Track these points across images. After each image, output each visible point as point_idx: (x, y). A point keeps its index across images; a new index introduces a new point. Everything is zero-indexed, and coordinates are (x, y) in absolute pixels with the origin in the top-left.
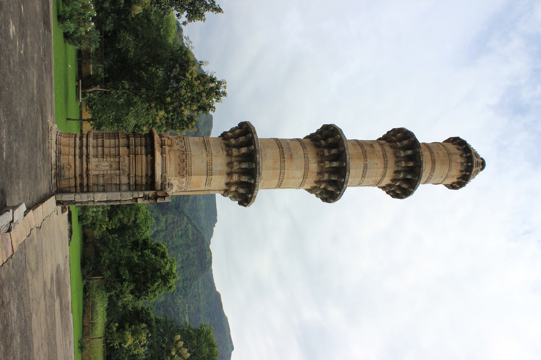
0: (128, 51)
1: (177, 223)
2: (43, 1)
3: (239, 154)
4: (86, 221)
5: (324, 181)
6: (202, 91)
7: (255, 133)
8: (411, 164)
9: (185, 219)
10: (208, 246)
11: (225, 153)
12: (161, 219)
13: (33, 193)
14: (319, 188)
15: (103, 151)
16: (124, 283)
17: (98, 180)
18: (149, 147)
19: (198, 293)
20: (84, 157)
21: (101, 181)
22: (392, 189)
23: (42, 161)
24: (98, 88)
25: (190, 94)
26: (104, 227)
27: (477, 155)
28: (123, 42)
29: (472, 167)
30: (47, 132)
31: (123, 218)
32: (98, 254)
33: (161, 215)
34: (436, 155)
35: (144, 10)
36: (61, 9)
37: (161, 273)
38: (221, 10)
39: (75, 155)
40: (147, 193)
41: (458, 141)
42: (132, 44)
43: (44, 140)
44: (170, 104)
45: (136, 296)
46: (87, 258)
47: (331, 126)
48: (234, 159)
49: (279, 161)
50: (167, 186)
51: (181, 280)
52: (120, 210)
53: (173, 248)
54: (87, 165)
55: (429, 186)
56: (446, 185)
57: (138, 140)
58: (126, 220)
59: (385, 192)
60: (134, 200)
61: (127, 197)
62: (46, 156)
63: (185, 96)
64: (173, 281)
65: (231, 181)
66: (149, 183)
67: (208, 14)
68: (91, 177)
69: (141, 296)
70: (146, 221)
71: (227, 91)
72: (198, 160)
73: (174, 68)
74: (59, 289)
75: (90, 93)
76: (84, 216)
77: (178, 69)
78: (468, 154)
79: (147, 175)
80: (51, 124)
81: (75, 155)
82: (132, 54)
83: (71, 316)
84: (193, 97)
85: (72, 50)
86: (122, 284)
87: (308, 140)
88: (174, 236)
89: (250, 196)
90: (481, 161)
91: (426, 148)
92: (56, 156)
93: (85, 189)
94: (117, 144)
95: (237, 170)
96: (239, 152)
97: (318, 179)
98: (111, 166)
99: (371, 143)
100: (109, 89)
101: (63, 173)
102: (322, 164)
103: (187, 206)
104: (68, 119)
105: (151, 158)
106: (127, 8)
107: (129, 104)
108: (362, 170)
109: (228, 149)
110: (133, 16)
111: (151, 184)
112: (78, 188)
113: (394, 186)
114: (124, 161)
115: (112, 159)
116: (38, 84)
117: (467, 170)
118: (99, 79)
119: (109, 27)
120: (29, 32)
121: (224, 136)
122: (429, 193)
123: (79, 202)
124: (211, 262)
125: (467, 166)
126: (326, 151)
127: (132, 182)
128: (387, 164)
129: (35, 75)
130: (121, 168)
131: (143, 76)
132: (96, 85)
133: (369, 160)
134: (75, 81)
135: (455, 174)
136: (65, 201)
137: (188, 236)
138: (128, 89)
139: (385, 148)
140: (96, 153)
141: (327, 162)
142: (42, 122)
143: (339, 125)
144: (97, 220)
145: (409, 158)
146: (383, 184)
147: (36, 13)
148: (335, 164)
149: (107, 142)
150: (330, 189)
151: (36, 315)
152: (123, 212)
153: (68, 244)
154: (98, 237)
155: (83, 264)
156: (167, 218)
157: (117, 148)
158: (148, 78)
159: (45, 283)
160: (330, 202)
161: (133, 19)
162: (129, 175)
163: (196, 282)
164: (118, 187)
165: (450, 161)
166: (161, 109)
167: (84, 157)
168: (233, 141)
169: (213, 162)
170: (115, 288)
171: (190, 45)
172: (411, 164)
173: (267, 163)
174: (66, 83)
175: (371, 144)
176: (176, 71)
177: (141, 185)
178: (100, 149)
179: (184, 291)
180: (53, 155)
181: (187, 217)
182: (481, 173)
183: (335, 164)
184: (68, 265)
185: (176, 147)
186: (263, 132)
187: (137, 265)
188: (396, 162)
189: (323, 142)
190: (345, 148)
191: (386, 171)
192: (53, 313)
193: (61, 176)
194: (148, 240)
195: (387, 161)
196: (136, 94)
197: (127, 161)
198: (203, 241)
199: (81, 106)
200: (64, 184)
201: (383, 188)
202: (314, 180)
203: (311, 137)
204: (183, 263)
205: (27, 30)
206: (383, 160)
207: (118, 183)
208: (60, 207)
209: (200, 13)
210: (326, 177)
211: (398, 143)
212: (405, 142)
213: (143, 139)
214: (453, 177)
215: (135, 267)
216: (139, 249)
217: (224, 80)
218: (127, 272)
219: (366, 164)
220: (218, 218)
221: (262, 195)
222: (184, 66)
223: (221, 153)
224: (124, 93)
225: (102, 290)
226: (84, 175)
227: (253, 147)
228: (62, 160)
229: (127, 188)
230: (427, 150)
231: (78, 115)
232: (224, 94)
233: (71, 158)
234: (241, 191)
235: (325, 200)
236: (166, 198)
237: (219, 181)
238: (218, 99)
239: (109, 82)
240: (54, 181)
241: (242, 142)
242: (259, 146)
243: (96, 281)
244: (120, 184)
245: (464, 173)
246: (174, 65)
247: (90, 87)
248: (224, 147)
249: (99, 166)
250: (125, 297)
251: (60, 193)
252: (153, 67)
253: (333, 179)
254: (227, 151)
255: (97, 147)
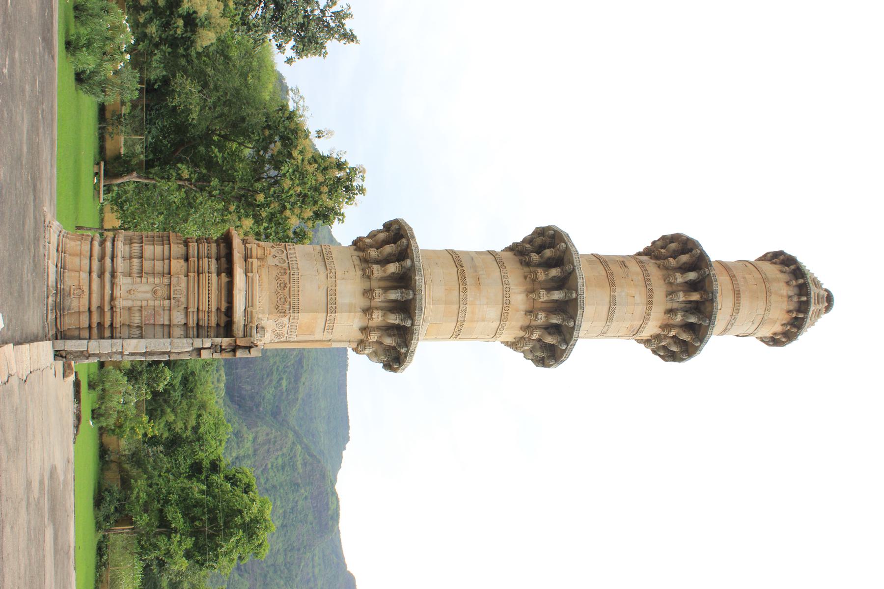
0: (188, 111)
1: (275, 442)
2: (42, 3)
3: (384, 275)
4: (106, 420)
5: (537, 327)
6: (321, 183)
7: (413, 237)
8: (695, 297)
9: (291, 434)
10: (333, 485)
11: (360, 273)
12: (246, 436)
13: (14, 321)
14: (529, 339)
15: (142, 266)
16: (173, 535)
17: (130, 319)
18: (223, 260)
19: (314, 576)
20: (107, 276)
21: (136, 319)
22: (663, 344)
23: (32, 275)
24: (134, 177)
25: (299, 189)
26: (140, 432)
27: (817, 284)
28: (179, 96)
29: (807, 304)
30: (42, 229)
31: (175, 422)
32: (126, 483)
33: (245, 428)
34: (740, 279)
35: (219, 39)
36: (73, 31)
37: (242, 517)
38: (355, 37)
39: (90, 273)
40: (218, 340)
41: (782, 257)
42: (196, 98)
43: (37, 240)
44: (261, 206)
45: (198, 562)
46: (106, 490)
47: (549, 228)
48: (375, 284)
49: (457, 289)
50: (254, 331)
51: (281, 550)
52: (169, 406)
53: (267, 490)
54: (112, 290)
55: (729, 338)
56: (762, 339)
57: (204, 247)
58: (180, 425)
59: (649, 351)
60: (195, 353)
61: (182, 347)
62: (38, 269)
63: (291, 192)
64: (263, 536)
65: (371, 324)
66: (222, 325)
67: (332, 45)
68: (118, 310)
69: (205, 561)
70: (217, 428)
71: (365, 185)
72: (311, 285)
73: (270, 143)
74: (53, 510)
75: (119, 185)
76: (102, 411)
77: (279, 144)
78: (801, 281)
79: (218, 309)
80: (49, 218)
81: (90, 273)
82: (195, 116)
83: (73, 574)
84: (305, 196)
85: (89, 104)
86: (169, 538)
87: (509, 254)
88: (269, 466)
89: (403, 351)
90: (826, 294)
91: (723, 269)
92: (57, 272)
93: (107, 333)
94: (166, 253)
95: (380, 305)
96: (384, 271)
97: (527, 323)
98: (155, 292)
99: (622, 259)
100: (153, 179)
101: (67, 303)
102: (532, 296)
103: (294, 412)
104: (79, 228)
105: (227, 280)
106: (189, 34)
107: (189, 204)
108: (606, 307)
109: (364, 265)
110: (200, 50)
111: (227, 328)
112: (95, 331)
113: (666, 336)
114: (178, 284)
115: (157, 280)
116: (29, 139)
117: (799, 311)
118: (134, 162)
119: (156, 72)
120: (17, 42)
121: (358, 244)
122: (730, 351)
123: (94, 355)
124: (338, 515)
125: (800, 303)
126: (540, 270)
127: (192, 322)
128: (651, 297)
129: (25, 121)
130: (172, 296)
131: (216, 156)
132: (129, 171)
133: (618, 290)
134: (92, 163)
135: (778, 316)
136: (70, 353)
137: (294, 468)
138: (186, 180)
139: (648, 268)
140: (127, 270)
141: (543, 292)
142: (35, 206)
143: (563, 226)
144: (126, 419)
145: (693, 286)
146: (646, 334)
147: (31, 17)
148: (557, 295)
149: (148, 250)
150: (549, 340)
151: (12, 528)
152: (174, 410)
153: (72, 441)
154: (127, 452)
155: (98, 501)
156: (257, 432)
157: (166, 261)
158: (224, 159)
159: (29, 484)
160: (549, 366)
161: (199, 54)
162: (187, 308)
163: (309, 555)
164: (167, 330)
165: (768, 293)
166: (247, 216)
167: (107, 276)
168: (373, 253)
169: (338, 288)
170: (155, 547)
171: (301, 103)
172: (695, 297)
173: (433, 293)
174: (77, 162)
175: (623, 262)
176: (276, 147)
177: (208, 327)
178: (136, 262)
179: (286, 571)
180: (52, 270)
181: (295, 432)
182: (825, 317)
183: (557, 295)
184: (70, 476)
185: (271, 261)
186: (426, 239)
187: (198, 504)
188: (669, 294)
189: (535, 257)
190: (574, 267)
191: (650, 309)
192: (41, 546)
193: (64, 309)
194: (220, 461)
195: (652, 290)
196: (202, 189)
197: (183, 285)
198: (323, 476)
199: (101, 211)
200: (69, 322)
201: (647, 342)
202: (520, 324)
203: (517, 250)
204: (284, 517)
205: (14, 38)
206: (644, 290)
207: (167, 323)
208: (60, 363)
209: (317, 43)
210: (541, 319)
211: (671, 260)
212: (684, 258)
213: (214, 245)
214: (775, 322)
215: (195, 506)
216: (203, 477)
217: (361, 166)
218: (180, 516)
219: (614, 297)
220: (352, 433)
221: (425, 350)
222: (289, 139)
223: (352, 273)
224: (180, 187)
225: (132, 554)
226: (107, 308)
227: (408, 262)
228: (66, 279)
229: (182, 332)
230: (725, 273)
231: (97, 219)
232: (362, 190)
233: (84, 276)
234: (389, 341)
235: (541, 362)
236: (252, 350)
237: (348, 324)
238: (349, 199)
239: (153, 166)
240: (51, 317)
241: (390, 255)
242: (421, 262)
243: (120, 536)
244: (169, 326)
245: (794, 315)
246: (271, 136)
247: (119, 175)
248: (357, 262)
249: (134, 293)
250: (175, 563)
251: (61, 339)
252: (234, 141)
253: (554, 321)
254: (363, 270)
255: (131, 258)
